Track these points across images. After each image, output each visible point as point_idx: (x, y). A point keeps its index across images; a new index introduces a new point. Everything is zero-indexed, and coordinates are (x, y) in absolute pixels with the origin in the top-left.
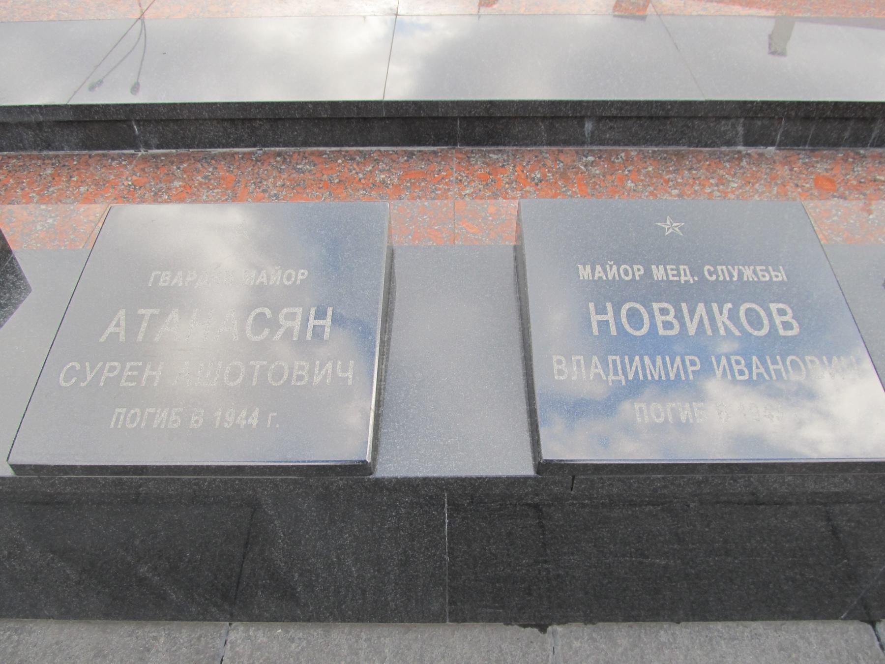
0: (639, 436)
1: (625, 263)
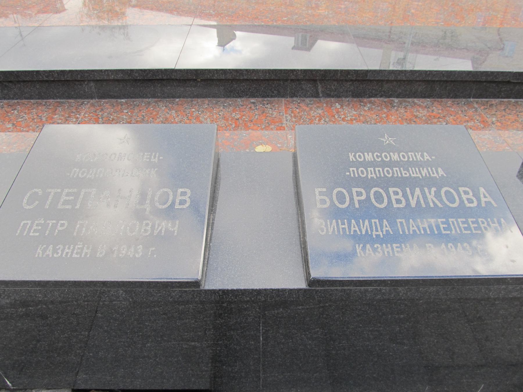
0: (369, 264)
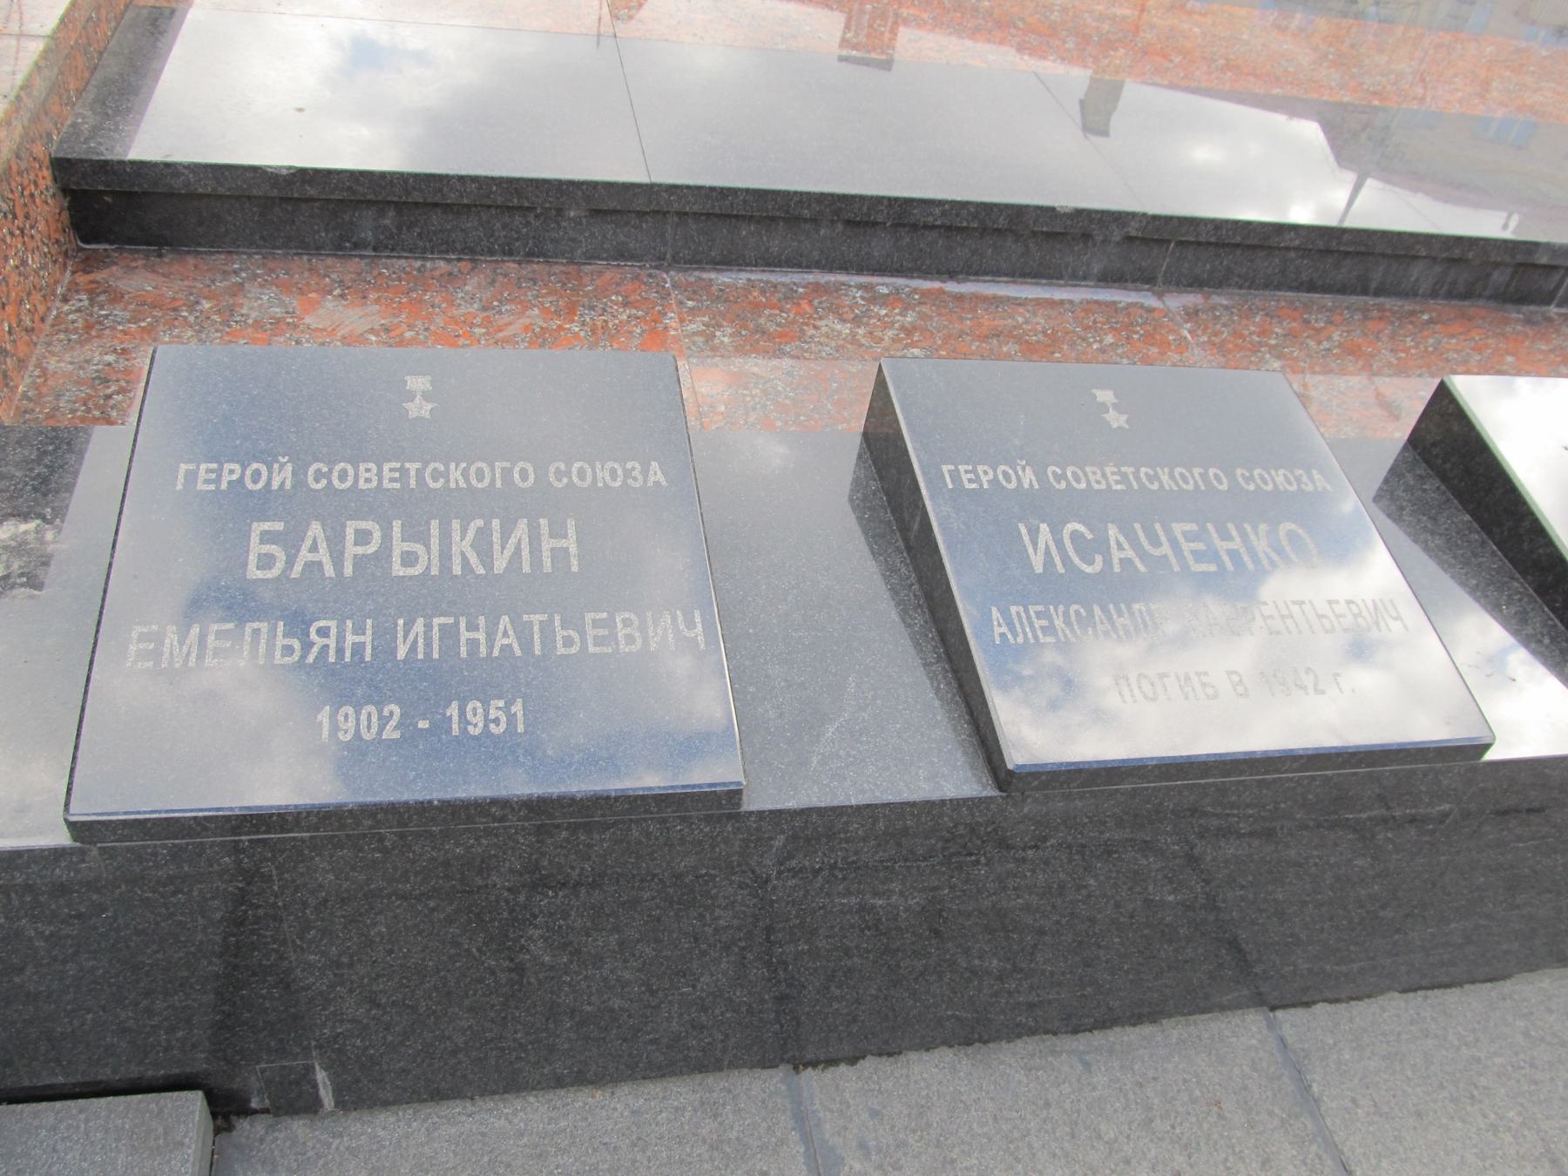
1: (256, 459)
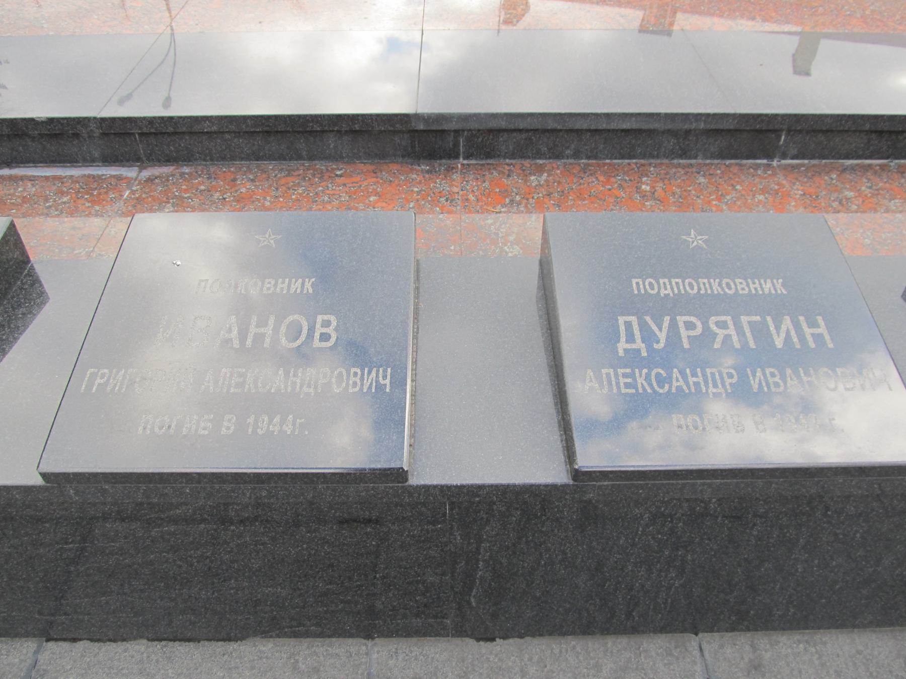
0: (657, 446)
